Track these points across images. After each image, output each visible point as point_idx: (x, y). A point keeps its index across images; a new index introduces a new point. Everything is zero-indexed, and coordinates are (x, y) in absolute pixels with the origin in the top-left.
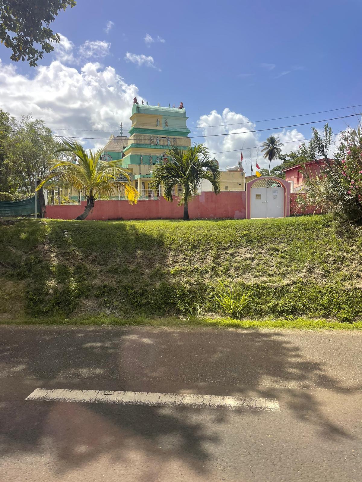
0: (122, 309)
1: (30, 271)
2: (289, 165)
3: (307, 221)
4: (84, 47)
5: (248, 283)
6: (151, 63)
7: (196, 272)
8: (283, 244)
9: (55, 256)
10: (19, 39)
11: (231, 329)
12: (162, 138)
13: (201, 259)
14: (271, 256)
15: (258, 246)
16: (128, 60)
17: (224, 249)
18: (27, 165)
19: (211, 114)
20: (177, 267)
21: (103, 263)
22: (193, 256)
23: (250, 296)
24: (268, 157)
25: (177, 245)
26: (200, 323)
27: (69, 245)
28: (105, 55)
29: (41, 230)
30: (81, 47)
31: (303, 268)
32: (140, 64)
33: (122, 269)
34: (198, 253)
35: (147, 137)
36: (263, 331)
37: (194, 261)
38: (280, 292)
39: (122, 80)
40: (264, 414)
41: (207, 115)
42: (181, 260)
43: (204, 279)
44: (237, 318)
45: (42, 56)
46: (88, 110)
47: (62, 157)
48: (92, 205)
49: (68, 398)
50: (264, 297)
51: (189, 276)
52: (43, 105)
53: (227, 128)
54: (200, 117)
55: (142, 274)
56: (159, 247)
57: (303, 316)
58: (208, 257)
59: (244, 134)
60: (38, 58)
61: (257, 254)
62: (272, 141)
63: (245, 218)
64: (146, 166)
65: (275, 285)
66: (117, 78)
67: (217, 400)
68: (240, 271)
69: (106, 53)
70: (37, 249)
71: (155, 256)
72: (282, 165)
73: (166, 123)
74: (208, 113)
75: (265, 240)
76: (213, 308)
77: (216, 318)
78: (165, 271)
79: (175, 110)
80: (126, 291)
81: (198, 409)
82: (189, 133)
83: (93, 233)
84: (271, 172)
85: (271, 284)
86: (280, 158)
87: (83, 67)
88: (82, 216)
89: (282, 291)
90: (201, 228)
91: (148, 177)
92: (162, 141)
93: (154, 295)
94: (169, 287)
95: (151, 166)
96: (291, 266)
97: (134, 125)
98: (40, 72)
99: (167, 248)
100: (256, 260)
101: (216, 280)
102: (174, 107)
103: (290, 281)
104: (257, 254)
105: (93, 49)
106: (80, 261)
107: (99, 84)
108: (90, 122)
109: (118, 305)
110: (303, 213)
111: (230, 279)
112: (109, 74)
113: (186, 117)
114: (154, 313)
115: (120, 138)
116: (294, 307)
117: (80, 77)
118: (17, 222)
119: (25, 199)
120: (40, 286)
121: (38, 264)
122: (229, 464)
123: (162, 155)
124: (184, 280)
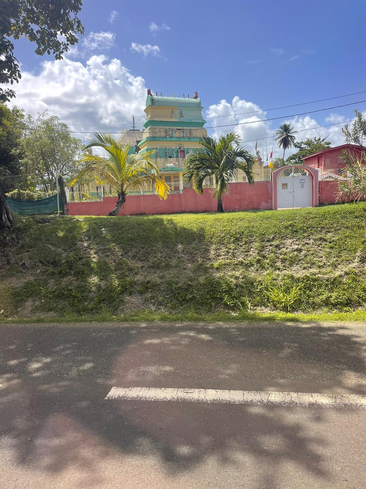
0: (168, 304)
1: (70, 268)
2: (306, 153)
3: (354, 209)
4: (89, 39)
5: (297, 276)
6: (157, 52)
7: (240, 265)
8: (330, 234)
9: (95, 253)
10: (42, 32)
11: (289, 324)
12: (178, 129)
13: (245, 252)
14: (319, 246)
15: (304, 237)
16: (134, 50)
17: (268, 241)
18: (46, 162)
19: (221, 103)
20: (221, 261)
21: (144, 258)
22: (236, 249)
23: (300, 289)
24: (282, 146)
25: (219, 238)
26: (253, 318)
27: (108, 241)
28: (110, 47)
29: (78, 227)
30: (85, 40)
31: (354, 258)
32: (145, 54)
33: (163, 264)
34: (241, 246)
35: (162, 130)
36: (325, 324)
37: (238, 254)
38: (333, 284)
39: (128, 72)
40: (362, 412)
41: (216, 105)
42: (223, 254)
43: (250, 273)
44: (287, 311)
45: (67, 48)
46: (94, 105)
47: (80, 153)
48: (124, 200)
49: (149, 396)
50: (315, 289)
51: (234, 269)
52: (49, 101)
53: (237, 116)
54: (209, 106)
55: (185, 269)
56: (200, 241)
57: (360, 308)
58: (252, 249)
59: (254, 122)
60: (63, 51)
61: (304, 245)
62: (286, 129)
63: (271, 209)
64: (163, 160)
65: (326, 277)
66: (123, 70)
67: (308, 398)
68: (287, 263)
69: (111, 45)
70: (77, 246)
71: (196, 250)
72: (298, 153)
73: (181, 114)
74: (217, 102)
75: (311, 230)
76: (262, 302)
77: (265, 312)
78: (208, 266)
79: (190, 100)
80: (170, 286)
81: (291, 407)
82: (204, 123)
83: (131, 229)
84: (287, 161)
85: (321, 276)
86: (296, 146)
87: (88, 60)
88: (114, 212)
89: (334, 283)
90: (241, 220)
91: (165, 171)
92: (177, 133)
93: (198, 290)
94: (214, 282)
95: (167, 159)
96: (341, 256)
97: (148, 118)
98: (45, 68)
99: (208, 242)
100: (304, 252)
101: (262, 273)
102: (189, 98)
103: (342, 273)
104: (304, 245)
105: (98, 41)
106: (120, 257)
107: (105, 78)
108: (97, 117)
109: (164, 301)
110: (12, 223)
111: (277, 272)
112: (115, 66)
113: (201, 107)
114: (201, 308)
115: (133, 131)
116: (349, 299)
117: (85, 70)
118: (52, 219)
119: (47, 197)
120: (83, 283)
121: (78, 261)
122: (345, 464)
123: (178, 148)
124: (229, 274)
